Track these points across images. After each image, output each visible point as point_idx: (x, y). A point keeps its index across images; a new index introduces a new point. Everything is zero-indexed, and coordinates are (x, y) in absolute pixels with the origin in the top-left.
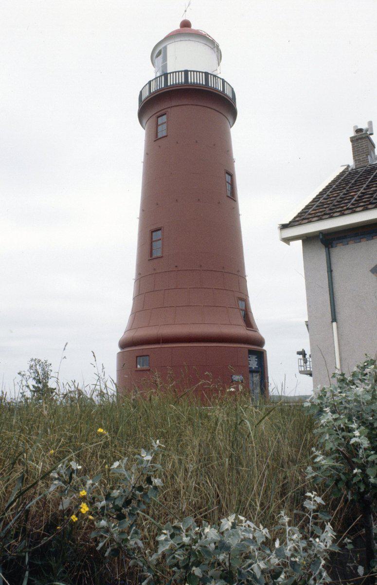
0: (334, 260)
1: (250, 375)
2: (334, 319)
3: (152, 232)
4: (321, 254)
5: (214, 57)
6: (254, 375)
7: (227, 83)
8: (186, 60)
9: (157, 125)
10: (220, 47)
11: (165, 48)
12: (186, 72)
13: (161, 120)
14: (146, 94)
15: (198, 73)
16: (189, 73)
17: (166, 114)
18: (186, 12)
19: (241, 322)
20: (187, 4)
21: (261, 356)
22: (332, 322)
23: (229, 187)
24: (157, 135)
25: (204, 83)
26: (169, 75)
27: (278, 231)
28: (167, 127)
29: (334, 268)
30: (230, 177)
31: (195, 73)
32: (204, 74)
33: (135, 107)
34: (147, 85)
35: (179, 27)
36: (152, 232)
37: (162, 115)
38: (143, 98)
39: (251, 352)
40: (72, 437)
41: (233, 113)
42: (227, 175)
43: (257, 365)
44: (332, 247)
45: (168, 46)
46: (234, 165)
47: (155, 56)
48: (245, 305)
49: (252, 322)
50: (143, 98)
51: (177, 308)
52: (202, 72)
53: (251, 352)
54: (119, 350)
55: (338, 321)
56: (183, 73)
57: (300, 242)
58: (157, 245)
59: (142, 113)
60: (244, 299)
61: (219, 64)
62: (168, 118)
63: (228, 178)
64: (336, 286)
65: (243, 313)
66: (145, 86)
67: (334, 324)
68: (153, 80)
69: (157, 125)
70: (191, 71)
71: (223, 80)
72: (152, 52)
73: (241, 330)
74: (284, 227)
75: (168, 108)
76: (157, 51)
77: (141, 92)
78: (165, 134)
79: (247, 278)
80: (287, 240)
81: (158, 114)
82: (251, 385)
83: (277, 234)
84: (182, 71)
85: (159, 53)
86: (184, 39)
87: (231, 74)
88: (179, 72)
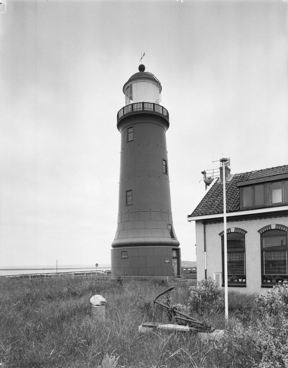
0: (206, 229)
1: (173, 260)
2: (205, 251)
3: (127, 192)
4: (202, 227)
5: (158, 90)
6: (175, 259)
7: (164, 108)
8: (144, 94)
9: (128, 133)
10: (161, 84)
11: (131, 85)
12: (143, 103)
13: (131, 130)
14: (121, 115)
15: (149, 104)
16: (145, 104)
17: (132, 127)
18: (141, 57)
19: (170, 236)
20: (143, 55)
21: (178, 251)
22: (204, 251)
23: (164, 167)
24: (128, 140)
25: (153, 110)
26: (134, 105)
27: (187, 218)
28: (133, 134)
29: (206, 232)
30: (165, 162)
31: (146, 104)
32: (152, 104)
33: (115, 122)
34: (122, 109)
35: (138, 71)
36: (127, 192)
37: (131, 128)
38: (120, 117)
39: (174, 249)
40: (170, 343)
41: (167, 125)
42: (163, 161)
43: (176, 255)
44: (206, 224)
45: (133, 85)
46: (169, 183)
47: (125, 89)
48: (171, 228)
49: (174, 235)
50: (120, 117)
51: (140, 230)
52: (152, 103)
53: (174, 249)
54: (112, 248)
55: (207, 251)
56: (142, 104)
57: (195, 221)
58: (129, 199)
59: (119, 125)
60: (171, 225)
61: (160, 93)
62: (133, 130)
63: (164, 163)
64: (206, 239)
65: (170, 231)
66: (121, 109)
67: (205, 252)
68: (125, 107)
69: (128, 133)
70: (146, 103)
71: (162, 107)
72: (123, 88)
73: (169, 240)
74: (189, 216)
75: (134, 124)
76: (127, 87)
77: (118, 112)
78: (132, 140)
79: (172, 214)
80: (190, 221)
81: (129, 126)
82: (173, 264)
83: (186, 219)
84: (141, 103)
85: (127, 88)
86: (141, 81)
87: (167, 101)
88: (139, 103)
